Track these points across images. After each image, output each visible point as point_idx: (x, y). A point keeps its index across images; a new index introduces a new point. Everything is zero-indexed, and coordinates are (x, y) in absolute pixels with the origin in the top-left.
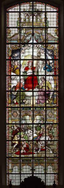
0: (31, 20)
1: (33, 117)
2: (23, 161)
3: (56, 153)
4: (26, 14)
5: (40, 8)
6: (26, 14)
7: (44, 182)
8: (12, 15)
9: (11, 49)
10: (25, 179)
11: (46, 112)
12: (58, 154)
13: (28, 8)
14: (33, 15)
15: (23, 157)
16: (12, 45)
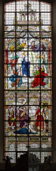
0: (26, 19)
1: (28, 99)
2: (31, 139)
3: (50, 133)
4: (21, 14)
5: (35, 8)
6: (21, 14)
7: (39, 158)
8: (9, 15)
9: (8, 42)
10: (21, 156)
11: (40, 94)
12: (52, 133)
13: (24, 8)
14: (28, 15)
15: (31, 136)
16: (9, 39)
